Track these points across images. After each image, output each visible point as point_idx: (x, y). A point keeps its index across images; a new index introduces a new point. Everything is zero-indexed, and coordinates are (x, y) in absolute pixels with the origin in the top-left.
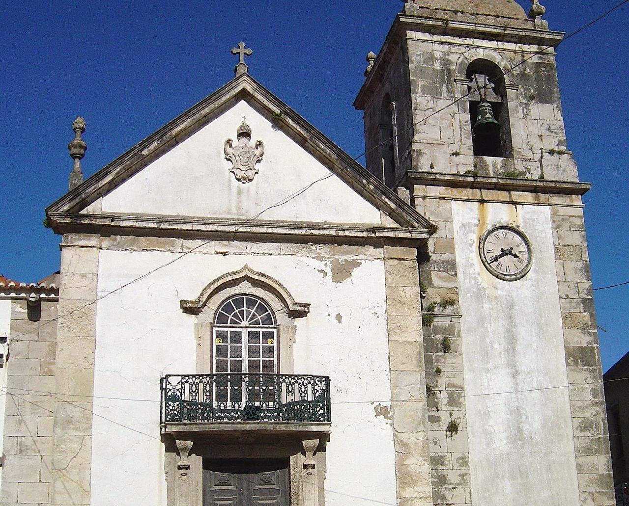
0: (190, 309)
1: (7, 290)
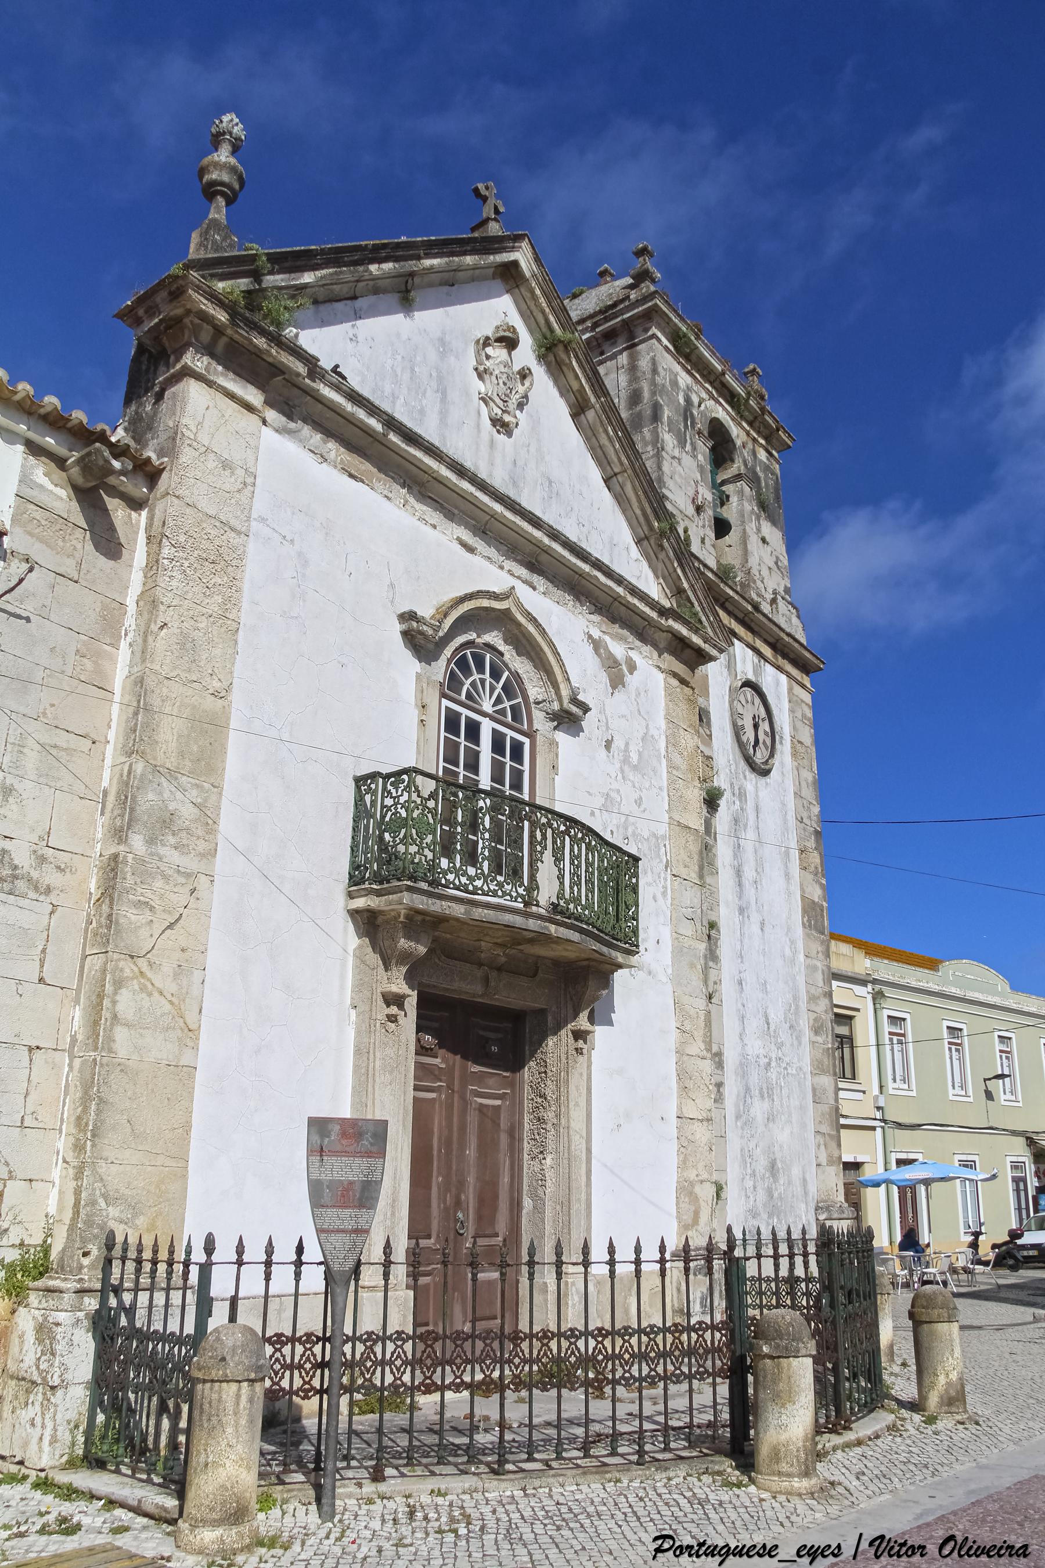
0: (420, 641)
1: (27, 409)
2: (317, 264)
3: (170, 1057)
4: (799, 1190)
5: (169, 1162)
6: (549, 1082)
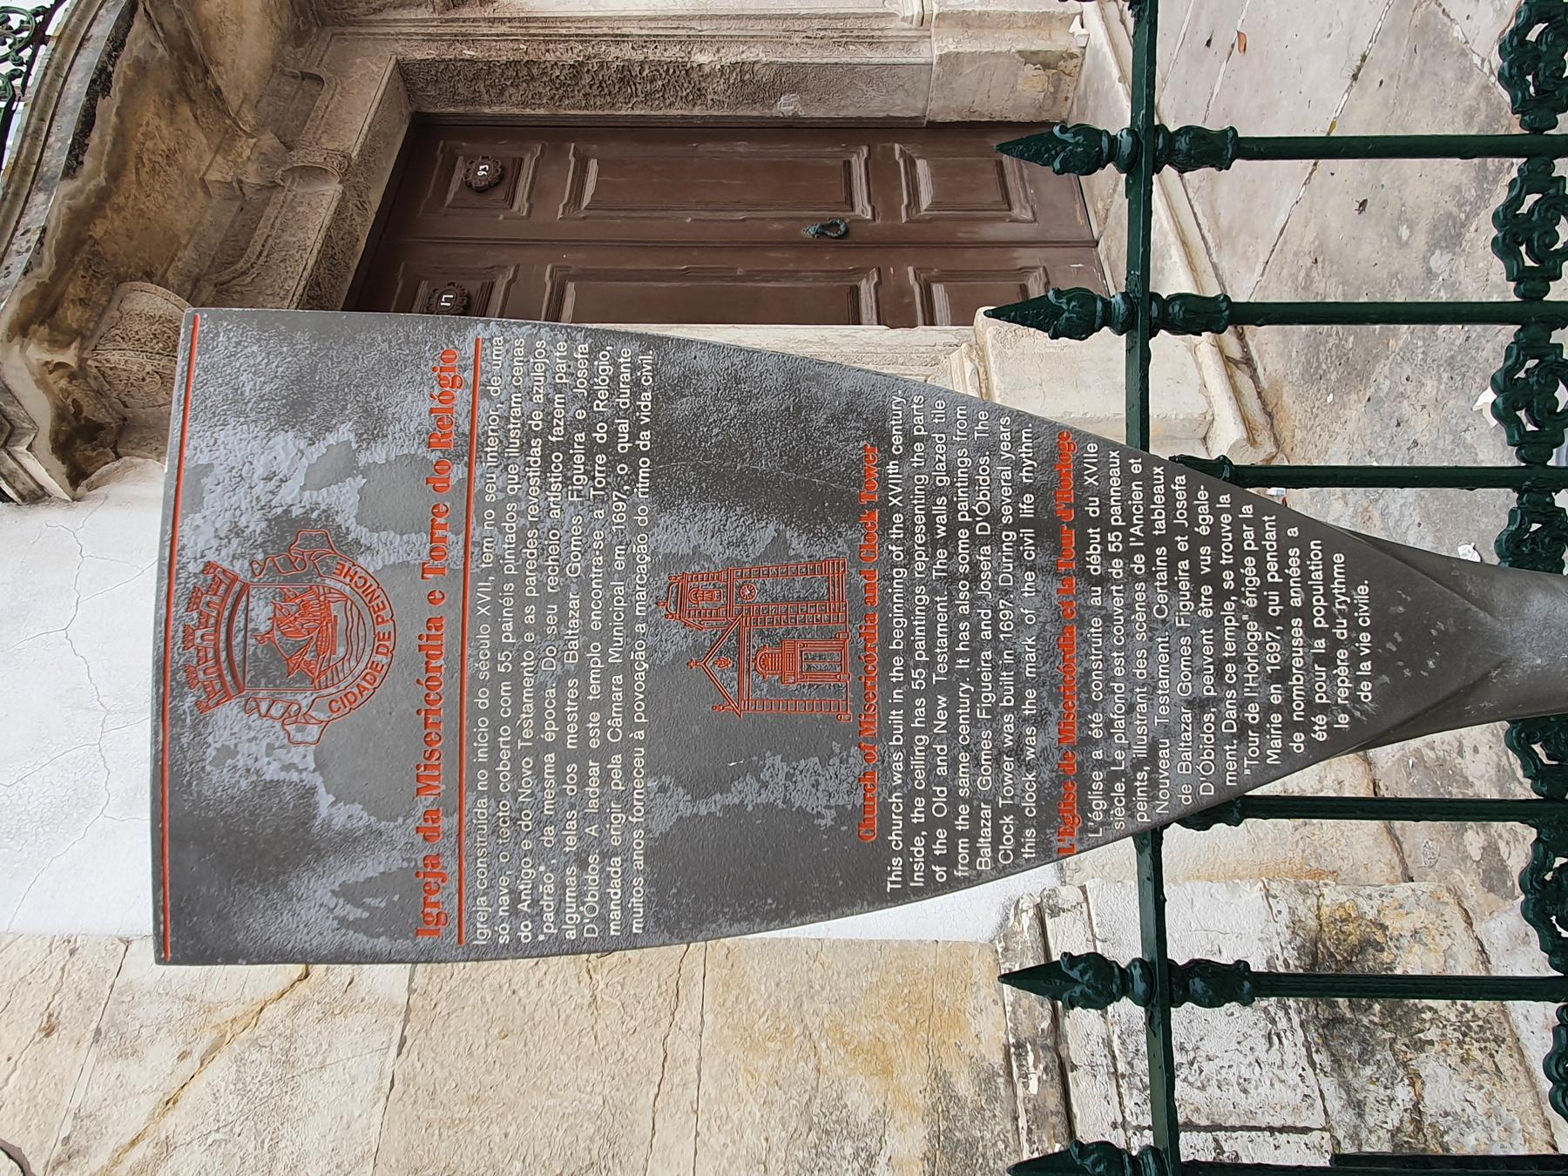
3: (378, 1039)
5: (688, 1016)
6: (550, 57)
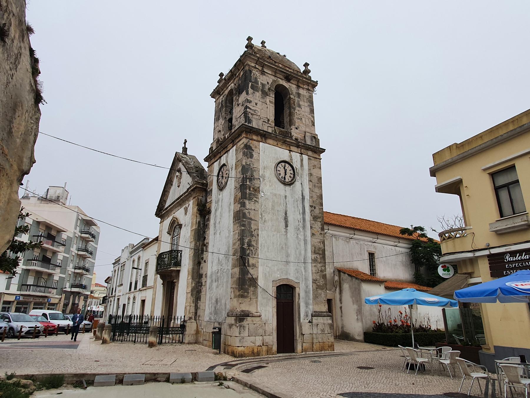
2: (27, 133)
4: (223, 307)
